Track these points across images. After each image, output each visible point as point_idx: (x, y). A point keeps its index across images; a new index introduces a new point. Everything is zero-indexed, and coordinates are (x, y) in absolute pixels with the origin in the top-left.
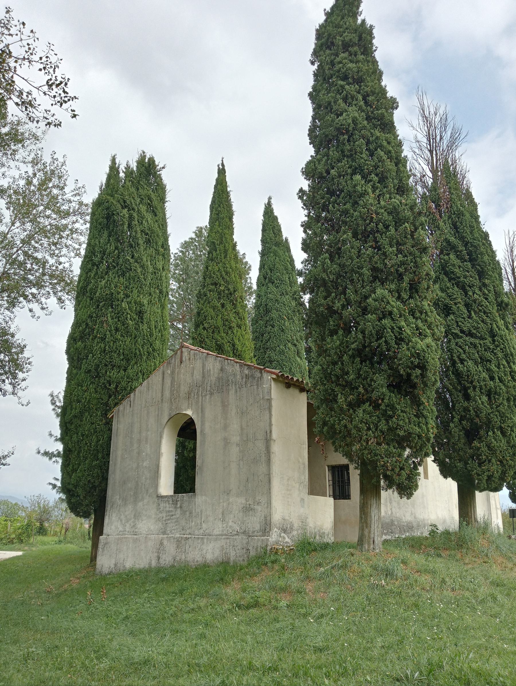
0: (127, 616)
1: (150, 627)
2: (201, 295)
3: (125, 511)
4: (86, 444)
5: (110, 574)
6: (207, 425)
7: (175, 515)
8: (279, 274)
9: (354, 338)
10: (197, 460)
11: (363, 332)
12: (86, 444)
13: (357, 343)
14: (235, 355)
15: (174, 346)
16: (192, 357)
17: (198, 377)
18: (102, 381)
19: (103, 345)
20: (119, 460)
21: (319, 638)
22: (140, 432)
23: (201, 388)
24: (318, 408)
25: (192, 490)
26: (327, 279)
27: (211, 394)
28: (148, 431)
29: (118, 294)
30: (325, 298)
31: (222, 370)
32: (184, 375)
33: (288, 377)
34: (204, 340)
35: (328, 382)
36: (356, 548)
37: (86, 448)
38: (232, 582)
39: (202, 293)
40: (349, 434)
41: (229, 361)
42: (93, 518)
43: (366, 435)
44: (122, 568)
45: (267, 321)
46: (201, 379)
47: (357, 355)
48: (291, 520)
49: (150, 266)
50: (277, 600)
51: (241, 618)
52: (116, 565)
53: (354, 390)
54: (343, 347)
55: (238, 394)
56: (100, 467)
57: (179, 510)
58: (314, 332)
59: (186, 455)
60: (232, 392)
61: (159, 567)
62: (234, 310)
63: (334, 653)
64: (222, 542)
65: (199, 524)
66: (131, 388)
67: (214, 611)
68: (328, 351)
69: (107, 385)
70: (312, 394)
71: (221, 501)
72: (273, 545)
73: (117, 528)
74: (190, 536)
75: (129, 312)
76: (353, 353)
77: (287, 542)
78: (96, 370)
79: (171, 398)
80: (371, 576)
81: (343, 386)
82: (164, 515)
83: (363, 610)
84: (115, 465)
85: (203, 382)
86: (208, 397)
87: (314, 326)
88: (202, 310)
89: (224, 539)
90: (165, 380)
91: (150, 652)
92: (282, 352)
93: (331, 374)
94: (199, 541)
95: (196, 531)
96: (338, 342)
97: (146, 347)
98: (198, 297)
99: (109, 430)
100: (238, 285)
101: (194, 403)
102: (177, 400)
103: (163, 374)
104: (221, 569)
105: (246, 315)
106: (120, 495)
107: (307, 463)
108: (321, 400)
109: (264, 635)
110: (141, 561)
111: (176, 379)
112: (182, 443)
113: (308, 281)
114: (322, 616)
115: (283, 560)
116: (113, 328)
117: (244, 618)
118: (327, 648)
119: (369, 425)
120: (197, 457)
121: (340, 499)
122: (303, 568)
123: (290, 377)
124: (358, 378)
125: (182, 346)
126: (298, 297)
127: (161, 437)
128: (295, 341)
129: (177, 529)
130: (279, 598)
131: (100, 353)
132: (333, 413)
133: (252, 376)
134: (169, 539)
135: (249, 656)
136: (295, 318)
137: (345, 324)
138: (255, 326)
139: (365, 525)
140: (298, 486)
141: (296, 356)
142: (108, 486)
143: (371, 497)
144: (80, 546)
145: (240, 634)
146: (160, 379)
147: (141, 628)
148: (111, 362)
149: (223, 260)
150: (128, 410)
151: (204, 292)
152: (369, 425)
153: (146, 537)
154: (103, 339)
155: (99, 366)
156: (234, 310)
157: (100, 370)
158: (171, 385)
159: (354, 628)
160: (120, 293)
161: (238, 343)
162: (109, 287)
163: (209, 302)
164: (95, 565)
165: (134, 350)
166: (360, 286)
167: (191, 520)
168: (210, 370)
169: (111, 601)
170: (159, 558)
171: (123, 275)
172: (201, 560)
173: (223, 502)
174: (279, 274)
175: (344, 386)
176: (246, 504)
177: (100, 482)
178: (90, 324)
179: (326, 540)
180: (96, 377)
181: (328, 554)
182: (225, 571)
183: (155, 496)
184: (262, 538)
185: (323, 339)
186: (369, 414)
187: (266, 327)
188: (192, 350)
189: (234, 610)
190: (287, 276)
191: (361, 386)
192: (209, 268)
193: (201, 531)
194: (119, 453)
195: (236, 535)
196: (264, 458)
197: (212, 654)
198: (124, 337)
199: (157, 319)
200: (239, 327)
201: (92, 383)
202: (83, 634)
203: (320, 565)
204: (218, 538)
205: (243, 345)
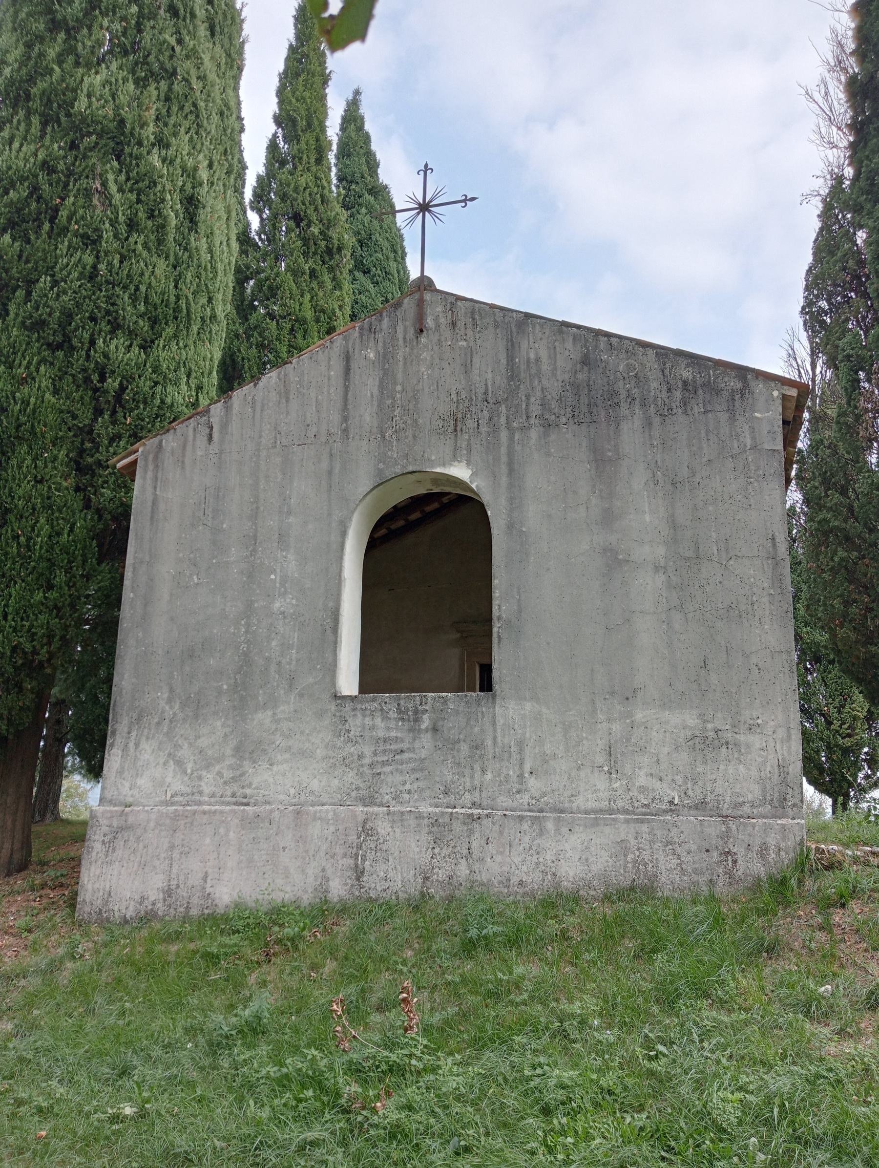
3: (198, 737)
8: (380, 256)
19: (88, 259)
22: (254, 516)
23: (503, 408)
52: (168, 892)
64: (625, 831)
71: (601, 717)
82: (368, 750)
86: (534, 434)
103: (347, 359)
106: (171, 690)
111: (400, 376)
129: (421, 790)
149: (314, 169)
157: (76, 330)
167: (477, 767)
168: (538, 360)
170: (359, 873)
173: (609, 720)
174: (380, 256)
176: (705, 729)
178: (46, 187)
193: (525, 799)
194: (166, 569)
195: (665, 812)
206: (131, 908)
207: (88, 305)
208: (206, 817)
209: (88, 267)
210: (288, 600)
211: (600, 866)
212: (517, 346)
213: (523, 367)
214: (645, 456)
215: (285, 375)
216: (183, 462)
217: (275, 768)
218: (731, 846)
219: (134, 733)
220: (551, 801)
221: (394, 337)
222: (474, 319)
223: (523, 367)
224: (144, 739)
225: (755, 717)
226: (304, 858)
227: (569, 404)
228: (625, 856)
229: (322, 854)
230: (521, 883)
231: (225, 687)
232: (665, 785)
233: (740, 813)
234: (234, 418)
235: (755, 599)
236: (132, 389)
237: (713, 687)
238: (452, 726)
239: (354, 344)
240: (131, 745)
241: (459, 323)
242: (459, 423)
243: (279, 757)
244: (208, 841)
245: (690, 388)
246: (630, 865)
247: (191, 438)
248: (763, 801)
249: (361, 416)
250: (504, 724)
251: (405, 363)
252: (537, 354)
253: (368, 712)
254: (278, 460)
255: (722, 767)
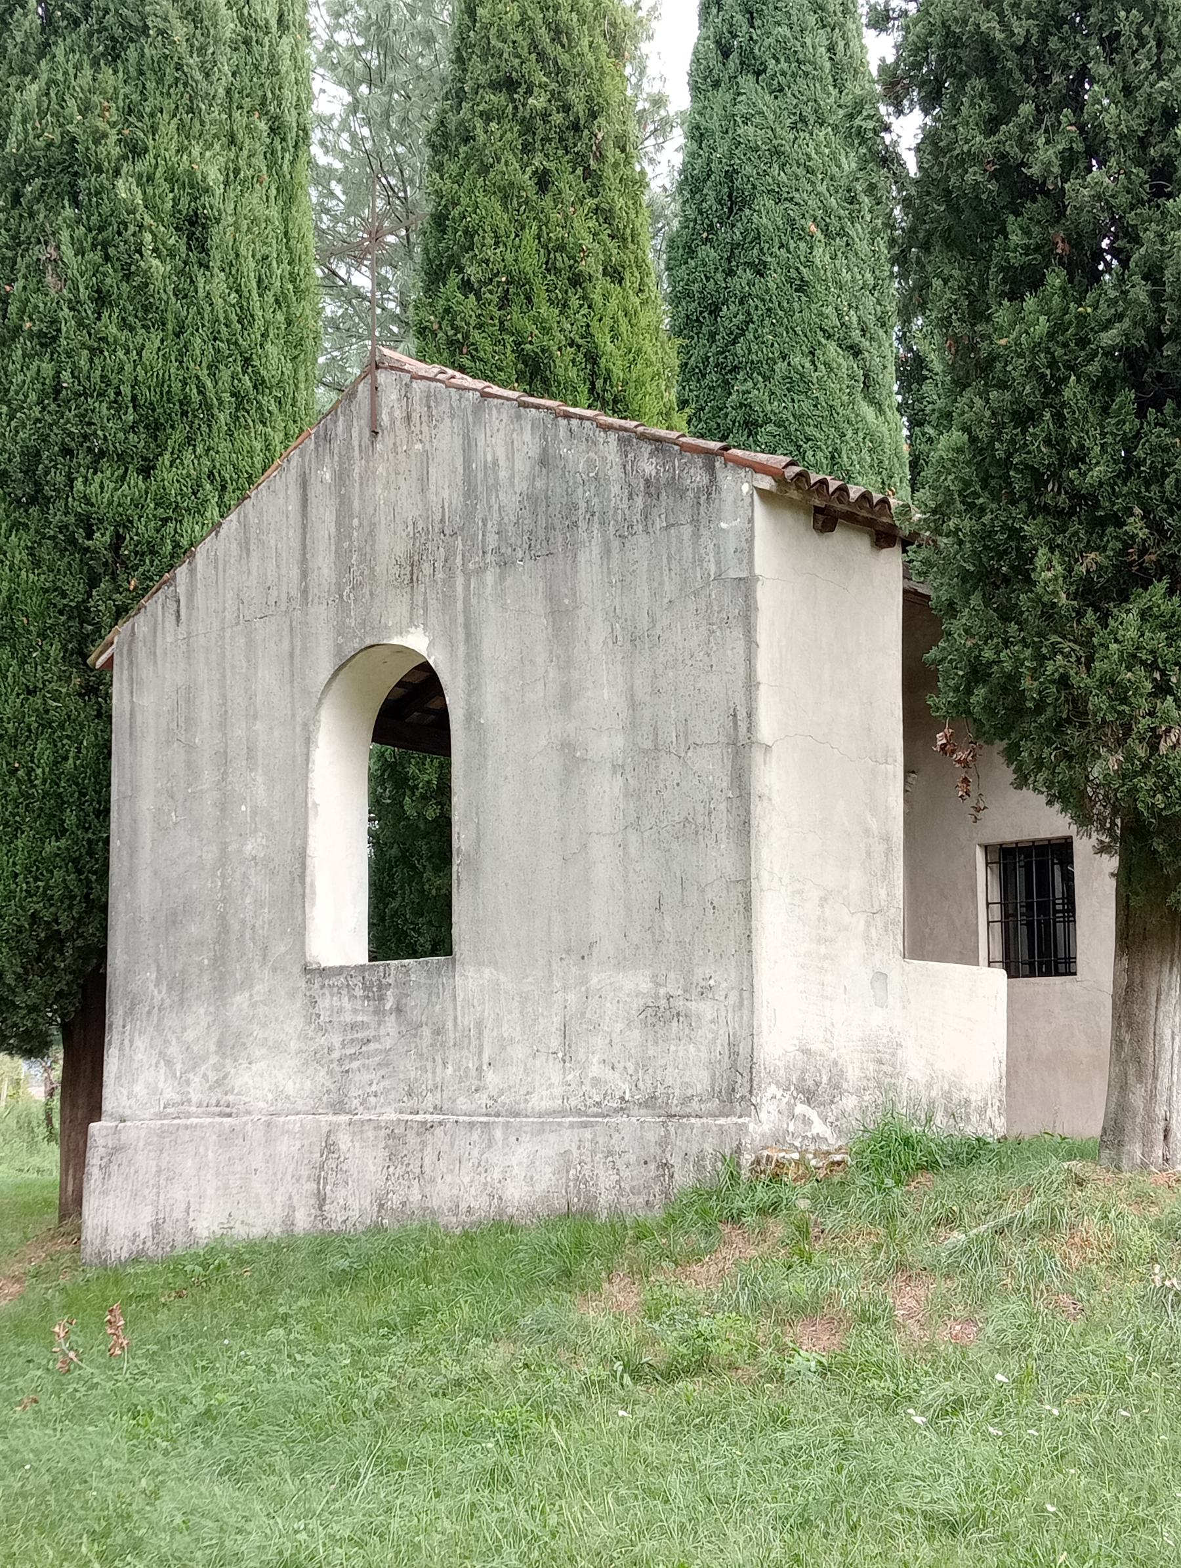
0: (208, 1411)
1: (298, 1449)
2: (446, 136)
3: (184, 1029)
4: (14, 772)
5: (136, 1261)
6: (491, 690)
7: (377, 1038)
8: (784, 30)
9: (1113, 303)
10: (455, 829)
11: (1153, 275)
12: (14, 772)
13: (1126, 323)
14: (597, 398)
15: (343, 369)
16: (419, 409)
17: (446, 494)
18: (56, 516)
19: (47, 368)
20: (147, 832)
21: (946, 1486)
22: (223, 725)
24: (952, 609)
25: (442, 945)
26: (999, 36)
27: (505, 564)
28: (255, 717)
29: (97, 142)
30: (992, 125)
31: (544, 461)
32: (387, 487)
33: (823, 482)
34: (466, 336)
35: (995, 498)
36: (1095, 1159)
37: (14, 789)
38: (606, 1285)
39: (452, 126)
40: (1078, 706)
41: (574, 422)
42: (61, 1055)
43: (1151, 714)
44: (180, 1238)
45: (735, 246)
46: (458, 501)
47: (1124, 379)
48: (834, 1055)
49: (224, 11)
50: (781, 1349)
51: (641, 1412)
52: (157, 1228)
53: (1104, 526)
54: (1065, 345)
55: (615, 564)
56: (75, 861)
57: (391, 1020)
58: (937, 283)
59: (410, 811)
60: (589, 555)
61: (322, 1232)
62: (590, 202)
63: (1005, 1537)
64: (567, 1139)
65: (474, 1073)
66: (176, 545)
67: (540, 1388)
68: (999, 365)
69: (80, 535)
70: (924, 553)
71: (557, 984)
72: (765, 1148)
73: (154, 1091)
74: (437, 1118)
75: (148, 220)
76: (1105, 370)
77: (816, 1139)
78: (29, 472)
79: (338, 584)
80: (1154, 1260)
81: (1059, 513)
82: (336, 1039)
83: (1122, 1384)
84: (132, 855)
85: (468, 514)
86: (490, 577)
87: (938, 258)
88: (455, 204)
89: (572, 1126)
90: (313, 512)
91: (303, 1536)
92: (797, 384)
93: (1006, 463)
94: (475, 1137)
95: (462, 1100)
96: (1043, 325)
97: (225, 374)
98: (433, 146)
99: (99, 715)
100: (608, 85)
101: (432, 602)
102: (366, 590)
103: (304, 484)
104: (562, 1237)
105: (642, 222)
106: (159, 969)
107: (900, 835)
108: (965, 576)
109: (734, 1475)
110: (252, 1212)
111: (356, 504)
112: (392, 766)
113: (916, 51)
114: (958, 1405)
115: (804, 1204)
116: (84, 294)
117: (657, 1414)
118: (981, 1518)
119: (1163, 674)
120: (456, 817)
121: (1032, 974)
122: (882, 1231)
123: (833, 485)
124: (1125, 476)
125: (376, 365)
126: (870, 124)
127: (308, 742)
128: (856, 334)
129: (387, 1091)
130: (787, 1340)
131: (40, 402)
132: (1013, 627)
133: (672, 483)
134: (357, 1128)
135: (677, 1549)
136: (856, 231)
137: (1075, 241)
138: (682, 271)
139: (1132, 1070)
140: (862, 926)
141: (859, 397)
142: (110, 933)
143: (1160, 963)
144: (17, 1164)
145: (641, 1469)
146: (293, 507)
147: (262, 1454)
148: (86, 437)
150: (169, 633)
151: (462, 122)
152: (1163, 674)
153: (268, 1124)
154: (47, 340)
155: (38, 454)
156: (590, 202)
157: (47, 473)
158: (338, 530)
159: (1085, 1451)
160: (105, 135)
161: (610, 347)
162: (56, 115)
163: (485, 170)
164: (79, 1229)
165: (176, 386)
166: (1145, 65)
168: (495, 462)
169: (145, 1356)
170: (321, 1200)
171: (114, 54)
172: (485, 1205)
173: (565, 988)
175: (1062, 516)
176: (657, 996)
177: (79, 921)
179: (972, 1129)
180: (33, 500)
181: (982, 1180)
182: (580, 1247)
183: (297, 969)
184: (722, 1121)
185: (978, 314)
186: (1164, 627)
187: (730, 273)
188: (415, 377)
189: (616, 1386)
190: (822, 37)
191: (1137, 511)
192: (480, 11)
193: (483, 1099)
194: (147, 804)
195: (616, 1111)
196: (722, 818)
197: (537, 1539)
198: (132, 329)
199: (265, 250)
200: (615, 274)
201: (15, 526)
202: (47, 1477)
203: (950, 1220)
204: (547, 1120)
205: (634, 355)
206: (125, 1249)
207: (56, 435)
208: (188, 1132)
209: (47, 381)
210: (259, 840)
211: (544, 1186)
212: (473, 443)
213: (480, 476)
214: (603, 602)
215: (245, 516)
216: (155, 653)
217: (254, 1067)
218: (668, 1156)
219: (128, 1027)
220: (508, 1101)
221: (349, 447)
222: (429, 407)
223: (480, 476)
224: (137, 1034)
225: (708, 976)
226: (273, 1183)
227: (525, 528)
228: (568, 1172)
229: (289, 1177)
230: (469, 1210)
231: (206, 962)
232: (617, 1075)
233: (688, 1110)
234: (199, 586)
235: (712, 806)
236: (132, 539)
237: (667, 936)
238: (415, 1001)
239: (310, 461)
240: (127, 1042)
241: (414, 414)
242: (415, 568)
243: (258, 1053)
244: (189, 1163)
245: (652, 490)
246: (571, 1184)
247: (160, 619)
248: (713, 1093)
249: (319, 568)
250: (464, 999)
251: (361, 484)
252: (494, 453)
253: (335, 989)
254: (242, 641)
255: (673, 1048)
